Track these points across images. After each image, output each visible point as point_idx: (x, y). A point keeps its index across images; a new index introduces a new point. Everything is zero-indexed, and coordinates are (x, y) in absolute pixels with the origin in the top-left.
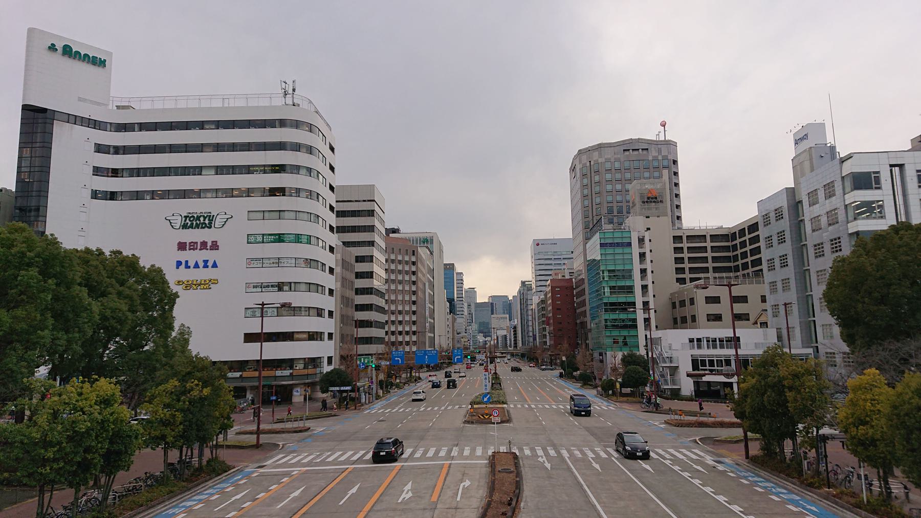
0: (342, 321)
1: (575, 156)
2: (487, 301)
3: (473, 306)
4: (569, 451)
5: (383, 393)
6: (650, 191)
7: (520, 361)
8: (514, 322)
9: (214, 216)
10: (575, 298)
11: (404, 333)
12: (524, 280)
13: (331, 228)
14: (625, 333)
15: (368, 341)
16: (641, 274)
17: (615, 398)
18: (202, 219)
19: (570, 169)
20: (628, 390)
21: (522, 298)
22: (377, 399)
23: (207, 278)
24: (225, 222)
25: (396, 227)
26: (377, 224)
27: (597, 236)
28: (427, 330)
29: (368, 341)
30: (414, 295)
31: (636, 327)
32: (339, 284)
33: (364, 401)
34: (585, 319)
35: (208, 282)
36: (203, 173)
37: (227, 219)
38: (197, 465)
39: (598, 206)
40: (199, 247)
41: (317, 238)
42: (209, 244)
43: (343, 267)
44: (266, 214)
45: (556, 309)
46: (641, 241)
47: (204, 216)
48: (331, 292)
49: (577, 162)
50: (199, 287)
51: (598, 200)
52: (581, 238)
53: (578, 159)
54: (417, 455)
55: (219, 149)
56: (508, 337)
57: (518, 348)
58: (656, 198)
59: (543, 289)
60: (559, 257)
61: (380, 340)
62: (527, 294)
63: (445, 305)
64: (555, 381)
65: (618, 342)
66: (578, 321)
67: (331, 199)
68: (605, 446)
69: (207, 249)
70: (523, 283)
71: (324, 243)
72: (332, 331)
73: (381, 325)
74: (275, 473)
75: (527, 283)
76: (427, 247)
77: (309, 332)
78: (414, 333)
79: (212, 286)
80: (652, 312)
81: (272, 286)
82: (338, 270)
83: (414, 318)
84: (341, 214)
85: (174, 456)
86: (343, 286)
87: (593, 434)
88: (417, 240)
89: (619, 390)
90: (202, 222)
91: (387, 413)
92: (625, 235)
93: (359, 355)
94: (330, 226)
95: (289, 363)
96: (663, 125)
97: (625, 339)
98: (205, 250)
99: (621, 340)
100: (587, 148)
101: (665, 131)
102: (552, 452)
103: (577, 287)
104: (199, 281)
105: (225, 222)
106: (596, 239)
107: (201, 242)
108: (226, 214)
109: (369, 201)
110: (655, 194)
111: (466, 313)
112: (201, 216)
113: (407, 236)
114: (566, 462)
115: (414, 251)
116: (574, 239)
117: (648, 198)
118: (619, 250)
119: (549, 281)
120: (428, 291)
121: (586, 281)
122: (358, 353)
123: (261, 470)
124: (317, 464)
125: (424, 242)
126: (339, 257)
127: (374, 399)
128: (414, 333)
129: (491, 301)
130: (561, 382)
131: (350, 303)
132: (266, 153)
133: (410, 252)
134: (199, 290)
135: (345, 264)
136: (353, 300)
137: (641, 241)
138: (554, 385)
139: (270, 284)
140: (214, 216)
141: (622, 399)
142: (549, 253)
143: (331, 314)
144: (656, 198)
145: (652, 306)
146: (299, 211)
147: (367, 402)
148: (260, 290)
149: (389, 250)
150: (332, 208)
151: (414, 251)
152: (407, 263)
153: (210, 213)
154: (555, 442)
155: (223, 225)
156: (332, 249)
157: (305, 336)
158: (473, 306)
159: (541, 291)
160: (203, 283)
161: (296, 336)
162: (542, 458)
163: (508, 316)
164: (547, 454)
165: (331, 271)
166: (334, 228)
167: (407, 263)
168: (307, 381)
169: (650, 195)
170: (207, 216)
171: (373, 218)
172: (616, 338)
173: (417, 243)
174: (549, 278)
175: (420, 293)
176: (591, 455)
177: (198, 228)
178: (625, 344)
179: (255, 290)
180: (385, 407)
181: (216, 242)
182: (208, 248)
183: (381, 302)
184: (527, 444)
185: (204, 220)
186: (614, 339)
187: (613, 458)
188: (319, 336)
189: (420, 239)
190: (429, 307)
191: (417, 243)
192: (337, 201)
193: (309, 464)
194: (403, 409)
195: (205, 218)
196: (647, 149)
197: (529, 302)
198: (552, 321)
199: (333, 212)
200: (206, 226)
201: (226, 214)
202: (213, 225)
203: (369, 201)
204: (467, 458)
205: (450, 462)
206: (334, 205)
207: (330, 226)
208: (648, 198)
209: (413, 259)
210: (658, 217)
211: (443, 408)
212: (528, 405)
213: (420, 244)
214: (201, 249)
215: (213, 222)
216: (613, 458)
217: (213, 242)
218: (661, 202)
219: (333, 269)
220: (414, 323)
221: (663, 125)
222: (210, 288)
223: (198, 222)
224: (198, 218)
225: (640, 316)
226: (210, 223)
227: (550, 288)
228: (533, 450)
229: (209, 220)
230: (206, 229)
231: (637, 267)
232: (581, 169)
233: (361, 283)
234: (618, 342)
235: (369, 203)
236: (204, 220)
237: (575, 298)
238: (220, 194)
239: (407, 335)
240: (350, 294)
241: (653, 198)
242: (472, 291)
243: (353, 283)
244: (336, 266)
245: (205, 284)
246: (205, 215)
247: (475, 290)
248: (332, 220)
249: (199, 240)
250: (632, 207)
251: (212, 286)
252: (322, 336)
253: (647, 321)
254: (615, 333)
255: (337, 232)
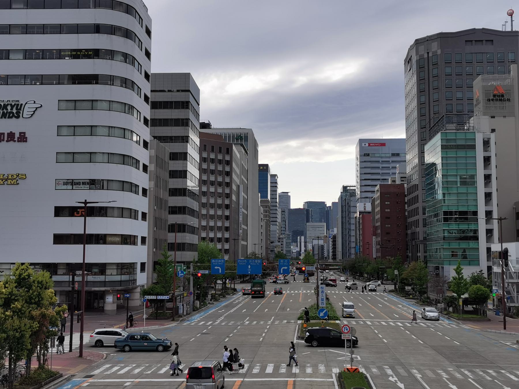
0: (156, 225)
1: (411, 46)
2: (302, 207)
3: (287, 211)
4: (420, 371)
5: (200, 304)
6: (496, 88)
7: (341, 274)
8: (333, 231)
9: (22, 104)
10: (406, 206)
11: (223, 240)
12: (345, 185)
13: (146, 121)
14: (464, 245)
15: (181, 247)
16: (485, 180)
17: (455, 315)
18: (9, 108)
19: (405, 61)
20: (470, 308)
21: (344, 204)
22: (194, 310)
23: (14, 172)
24: (34, 112)
25: (206, 122)
26: (192, 117)
27: (438, 137)
28: (240, 238)
29: (181, 247)
30: (227, 198)
31: (476, 238)
32: (153, 183)
33: (182, 312)
34: (418, 230)
35: (15, 176)
36: (11, 57)
37: (37, 108)
38: (23, 372)
39: (436, 103)
40: (6, 139)
41: (131, 131)
42: (17, 135)
43: (157, 165)
44: (78, 104)
45: (385, 218)
46: (486, 143)
47: (11, 105)
48: (145, 191)
49: (413, 53)
50: (6, 183)
51: (436, 96)
52: (415, 139)
53: (414, 50)
54: (256, 371)
55: (45, 30)
56: (325, 248)
57: (338, 260)
58: (503, 96)
59: (369, 195)
60: (388, 160)
61: (192, 247)
62: (351, 201)
63: (259, 210)
64: (386, 297)
65: (456, 256)
66: (409, 232)
67: (146, 88)
68: (458, 367)
69: (15, 141)
70: (345, 188)
71: (138, 137)
72: (146, 235)
73: (193, 230)
74: (105, 384)
75: (348, 188)
76: (242, 145)
77: (122, 235)
78: (227, 240)
79: (20, 181)
80: (495, 222)
81: (84, 183)
82: (151, 168)
83: (227, 224)
84: (155, 105)
85: (474, 306)
86: (157, 185)
87: (441, 353)
88: (229, 137)
89: (461, 308)
90: (9, 111)
91: (209, 325)
92: (469, 136)
93: (178, 262)
94: (145, 119)
95: (102, 268)
96: (511, 14)
97: (464, 251)
98: (12, 142)
99: (460, 253)
100: (424, 38)
101: (512, 21)
102: (401, 371)
103: (409, 194)
104: (6, 175)
105: (34, 112)
106: (437, 140)
107: (8, 134)
108: (35, 103)
109: (183, 91)
110: (501, 91)
111: (279, 220)
112: (8, 104)
113: (219, 132)
114: (419, 382)
115: (228, 149)
116: (409, 137)
117: (494, 96)
118: (461, 153)
119: (378, 187)
120: (242, 194)
121: (420, 188)
122: (177, 260)
123: (91, 380)
124: (147, 376)
125: (237, 139)
126: (153, 152)
127: (192, 310)
128: (227, 240)
129: (306, 208)
130: (394, 298)
131: (163, 205)
132: (92, 35)
133: (224, 150)
134: (6, 185)
135: (158, 160)
136: (166, 202)
137: (486, 143)
138: (368, 301)
139: (81, 181)
140: (22, 104)
141: (465, 316)
142: (376, 155)
143: (144, 215)
144: (503, 96)
145: (495, 215)
146: (112, 101)
147: (185, 313)
148: (70, 187)
149: (203, 148)
150: (146, 99)
151: (228, 149)
152: (220, 162)
153: (18, 101)
154: (403, 361)
155: (32, 115)
156: (146, 145)
157: (118, 239)
158: (287, 211)
159: (367, 198)
160: (10, 177)
161: (109, 239)
162: (393, 377)
163: (325, 224)
164: (397, 374)
165: (145, 168)
166: (148, 120)
167: (220, 162)
168: (120, 288)
169: (496, 92)
170: (15, 104)
171: (188, 110)
172: (455, 251)
173: (229, 140)
174: (378, 183)
175: (234, 198)
176: (445, 376)
177: (5, 118)
178: (465, 257)
179: (65, 187)
180: (206, 319)
181: (24, 133)
182: (16, 139)
183: (194, 205)
184: (373, 363)
185: (12, 109)
186: (453, 252)
187: (470, 380)
188: (132, 239)
189: (233, 136)
190: (243, 212)
191: (229, 140)
192: (152, 91)
193: (140, 375)
194: (203, 323)
195: (12, 107)
196: (492, 41)
197: (352, 210)
198: (379, 231)
199: (148, 103)
200: (13, 116)
201: (35, 103)
202: (21, 115)
203: (183, 91)
204: (310, 376)
205: (294, 379)
206: (149, 94)
207: (145, 119)
208: (494, 96)
209: (227, 158)
210: (505, 117)
211: (269, 322)
212: (363, 321)
213: (233, 141)
214: (7, 141)
215: (21, 112)
216: (470, 380)
217: (20, 133)
218: (509, 100)
219: (147, 166)
220: (227, 229)
221: (511, 14)
222: (18, 184)
223: (5, 111)
224: (5, 106)
225: (482, 227)
226: (18, 113)
227: (379, 194)
228: (380, 368)
229: (17, 109)
230: (14, 118)
231: (480, 172)
232: (418, 62)
233: (175, 183)
234: (456, 256)
235: (184, 93)
236: (12, 109)
237: (406, 206)
238: (28, 81)
239: (219, 242)
240: (164, 194)
241: (499, 96)
242: (286, 197)
243: (166, 182)
244: (150, 163)
245: (12, 179)
246: (13, 104)
247: (289, 194)
248: (146, 111)
249: (6, 131)
250: (476, 105)
251: (20, 181)
252: (136, 240)
253: (489, 232)
254: (455, 245)
255: (152, 126)
